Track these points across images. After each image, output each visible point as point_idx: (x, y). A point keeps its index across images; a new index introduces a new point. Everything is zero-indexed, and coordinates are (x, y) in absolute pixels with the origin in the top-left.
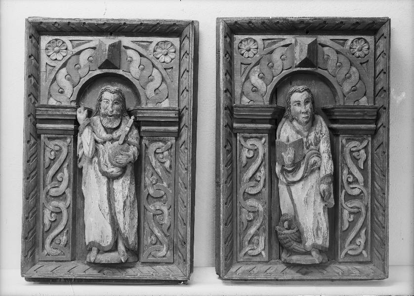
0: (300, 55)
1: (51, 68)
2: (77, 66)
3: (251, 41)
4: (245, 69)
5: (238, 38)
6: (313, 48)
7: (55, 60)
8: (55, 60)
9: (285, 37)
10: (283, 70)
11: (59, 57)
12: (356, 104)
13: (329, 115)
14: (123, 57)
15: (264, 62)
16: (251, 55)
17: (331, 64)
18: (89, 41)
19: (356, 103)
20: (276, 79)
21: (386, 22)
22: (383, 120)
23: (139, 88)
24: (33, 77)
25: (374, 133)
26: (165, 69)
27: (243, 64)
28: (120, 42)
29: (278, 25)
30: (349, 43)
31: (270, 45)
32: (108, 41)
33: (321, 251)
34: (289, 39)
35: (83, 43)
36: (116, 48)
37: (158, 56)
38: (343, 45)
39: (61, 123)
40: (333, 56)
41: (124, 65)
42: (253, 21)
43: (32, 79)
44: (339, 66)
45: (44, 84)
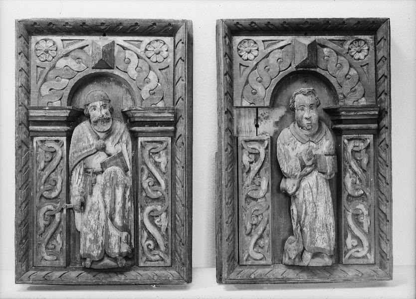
0: (302, 56)
1: (42, 69)
2: (266, 68)
3: (356, 43)
4: (244, 70)
5: (237, 39)
6: (313, 48)
7: (246, 60)
8: (246, 60)
9: (281, 38)
10: (280, 71)
11: (251, 56)
12: (355, 104)
13: (126, 117)
14: (320, 54)
15: (261, 66)
16: (362, 57)
17: (332, 66)
18: (279, 41)
19: (355, 102)
20: (274, 82)
21: (386, 21)
22: (384, 122)
23: (336, 86)
24: (229, 75)
25: (377, 133)
26: (160, 70)
27: (162, 69)
28: (113, 42)
29: (36, 26)
30: (143, 46)
31: (268, 46)
32: (101, 41)
33: (127, 257)
34: (287, 39)
35: (275, 43)
36: (109, 52)
37: (353, 54)
38: (342, 45)
39: (55, 125)
40: (334, 58)
41: (322, 65)
42: (271, 22)
43: (227, 76)
44: (340, 67)
45: (239, 81)
